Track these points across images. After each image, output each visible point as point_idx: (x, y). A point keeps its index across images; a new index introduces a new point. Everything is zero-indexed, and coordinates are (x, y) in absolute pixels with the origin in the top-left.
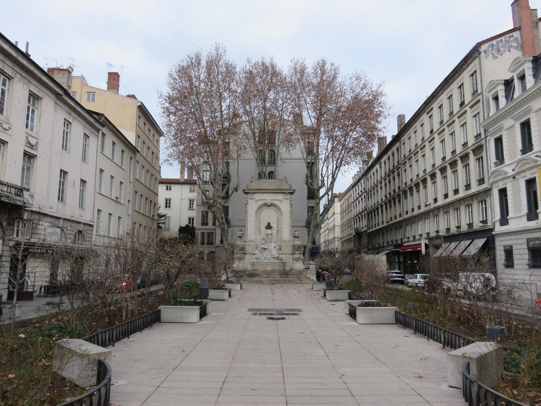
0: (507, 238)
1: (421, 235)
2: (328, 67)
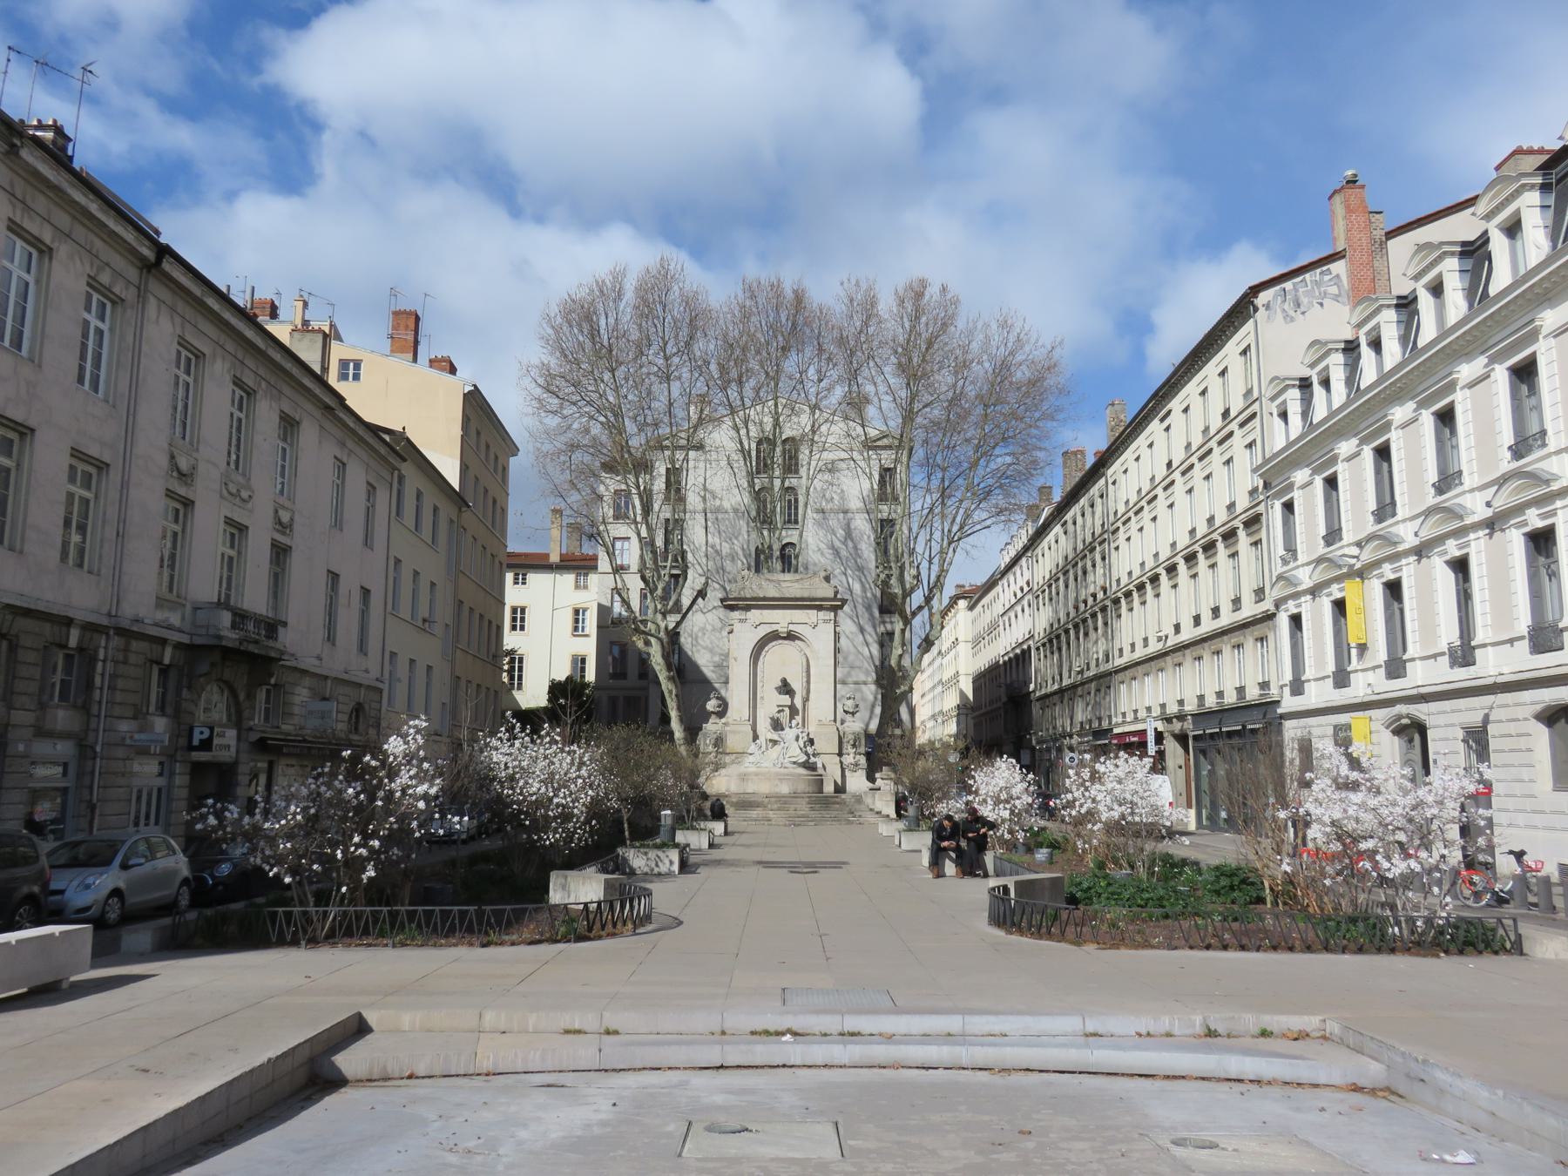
1: (1149, 709)
2: (933, 292)
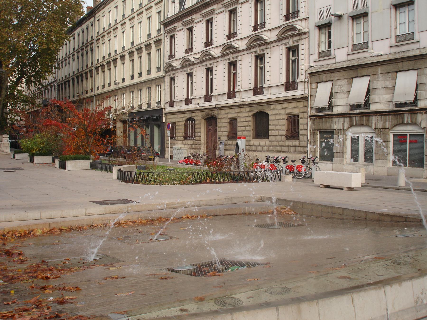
0: (232, 111)
